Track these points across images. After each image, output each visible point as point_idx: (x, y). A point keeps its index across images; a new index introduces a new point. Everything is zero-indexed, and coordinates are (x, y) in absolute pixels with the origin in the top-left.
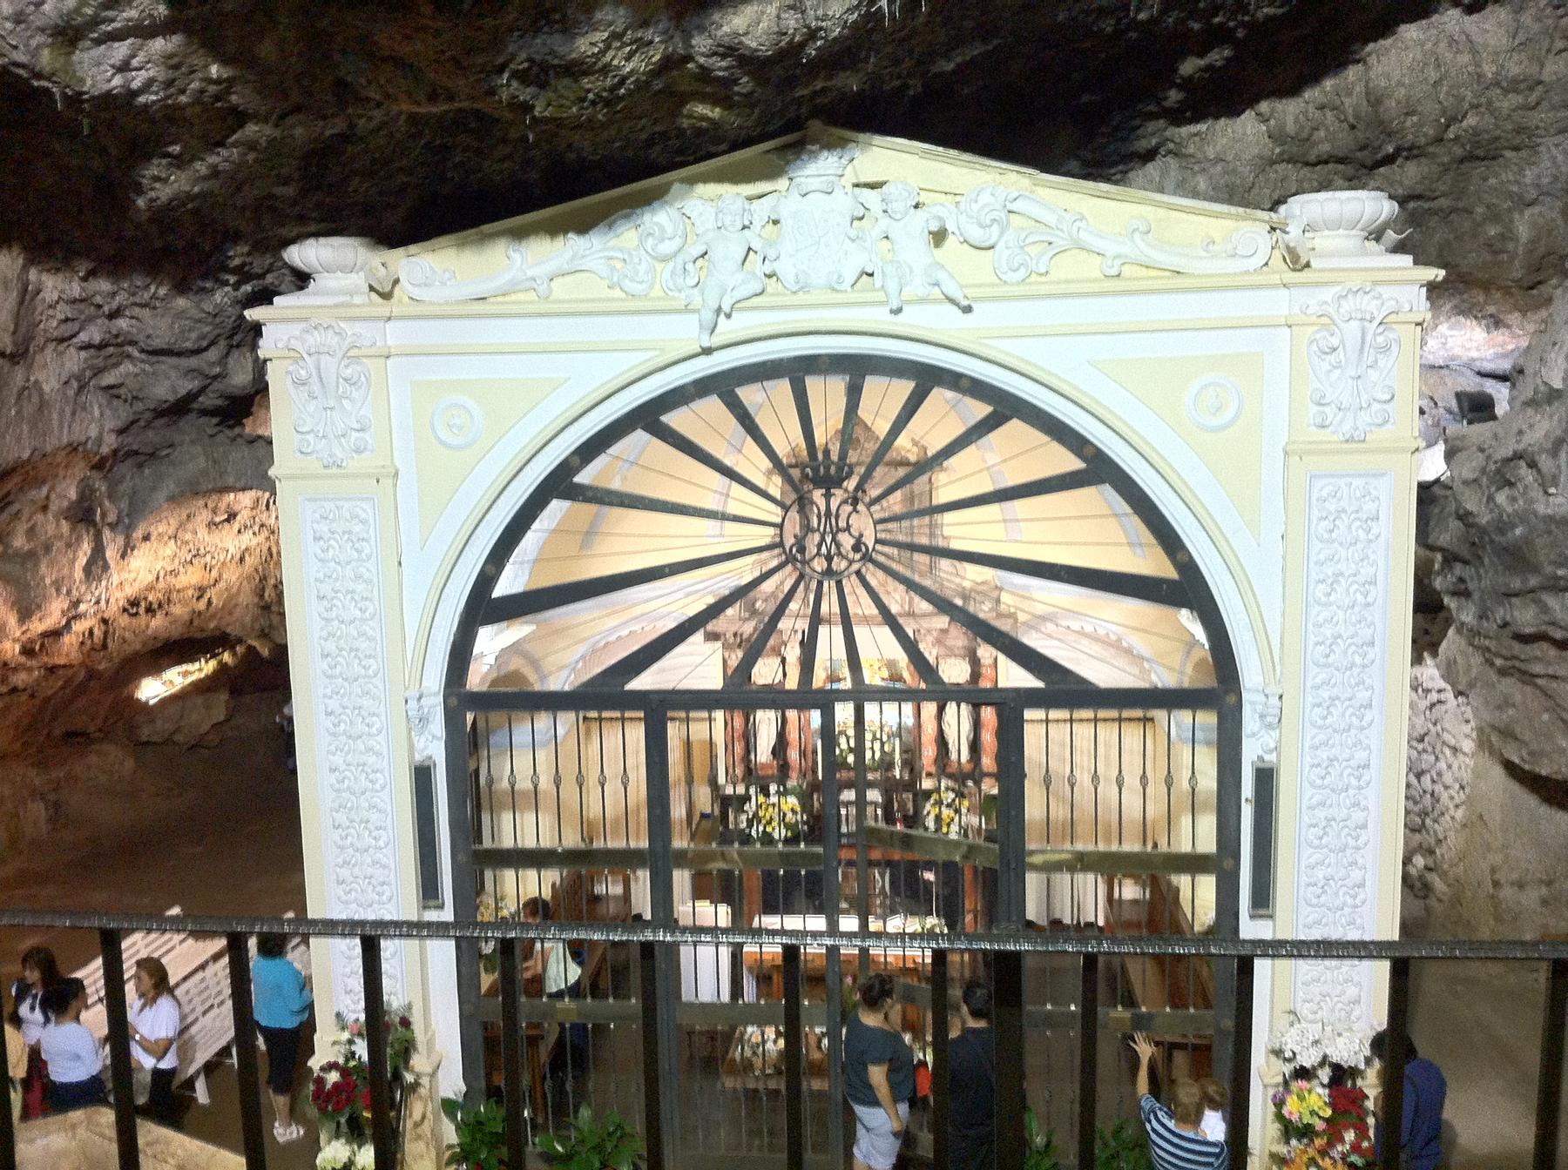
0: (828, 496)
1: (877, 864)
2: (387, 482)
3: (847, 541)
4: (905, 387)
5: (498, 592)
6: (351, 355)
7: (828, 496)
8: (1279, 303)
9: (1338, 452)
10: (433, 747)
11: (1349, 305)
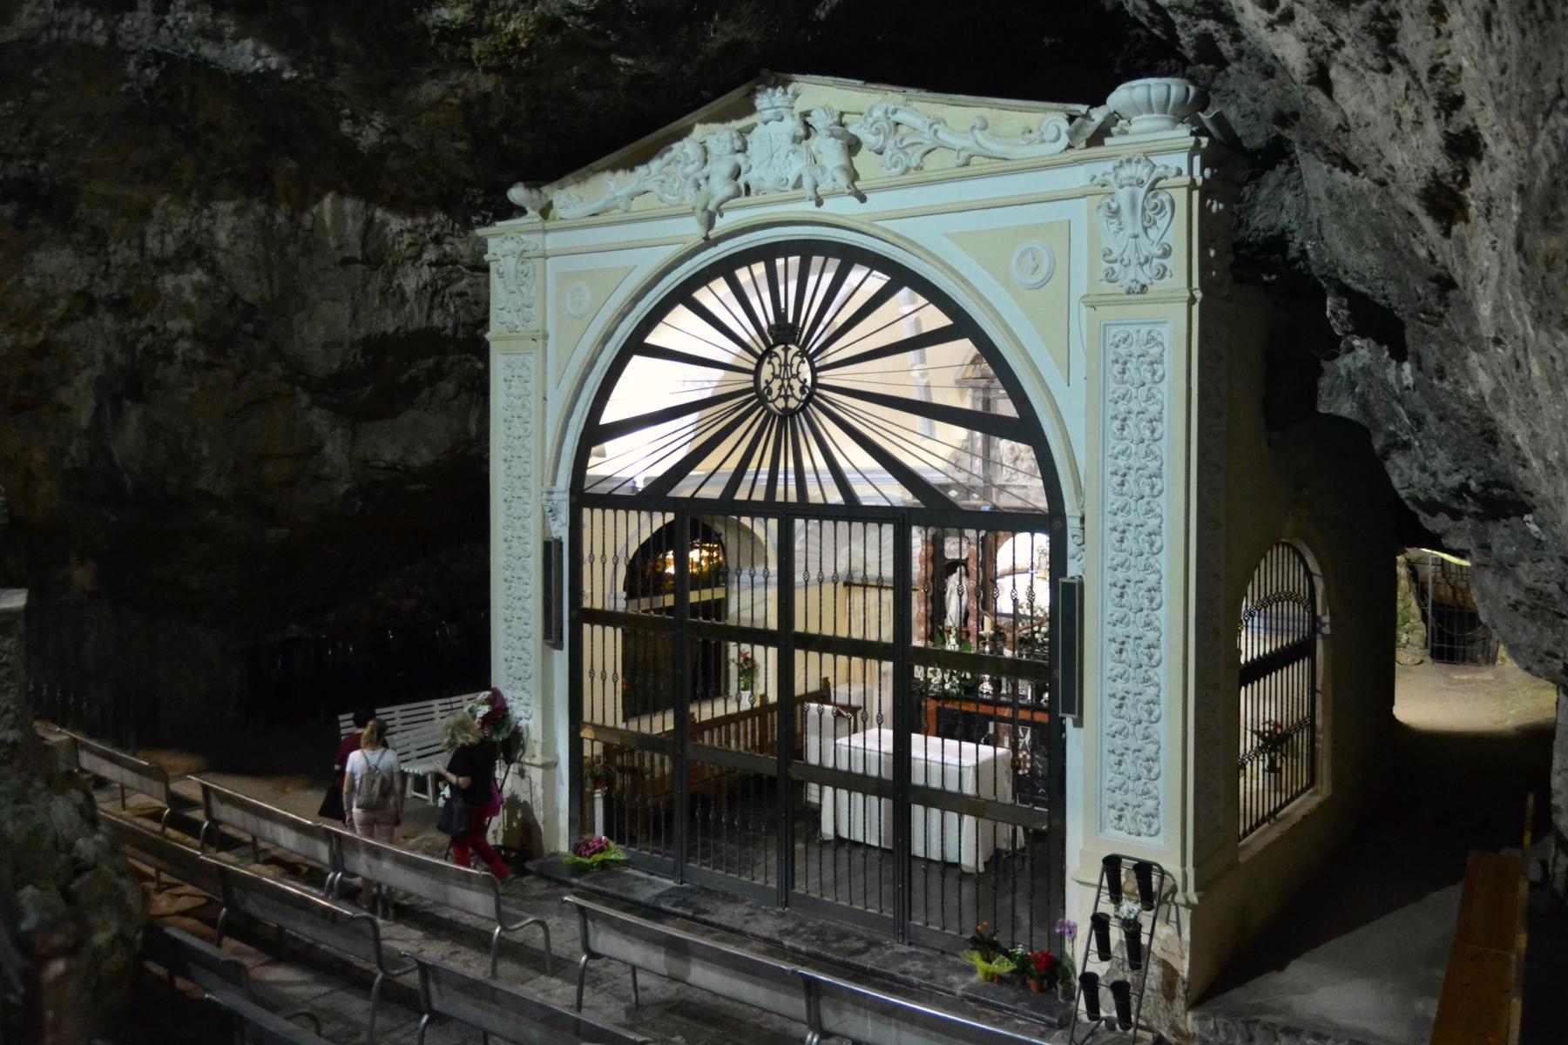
0: (786, 350)
1: (1024, 723)
2: (540, 341)
3: (796, 384)
4: (878, 281)
5: (604, 420)
6: (523, 256)
7: (786, 350)
8: (1078, 177)
9: (1116, 303)
10: (561, 530)
11: (1127, 172)
